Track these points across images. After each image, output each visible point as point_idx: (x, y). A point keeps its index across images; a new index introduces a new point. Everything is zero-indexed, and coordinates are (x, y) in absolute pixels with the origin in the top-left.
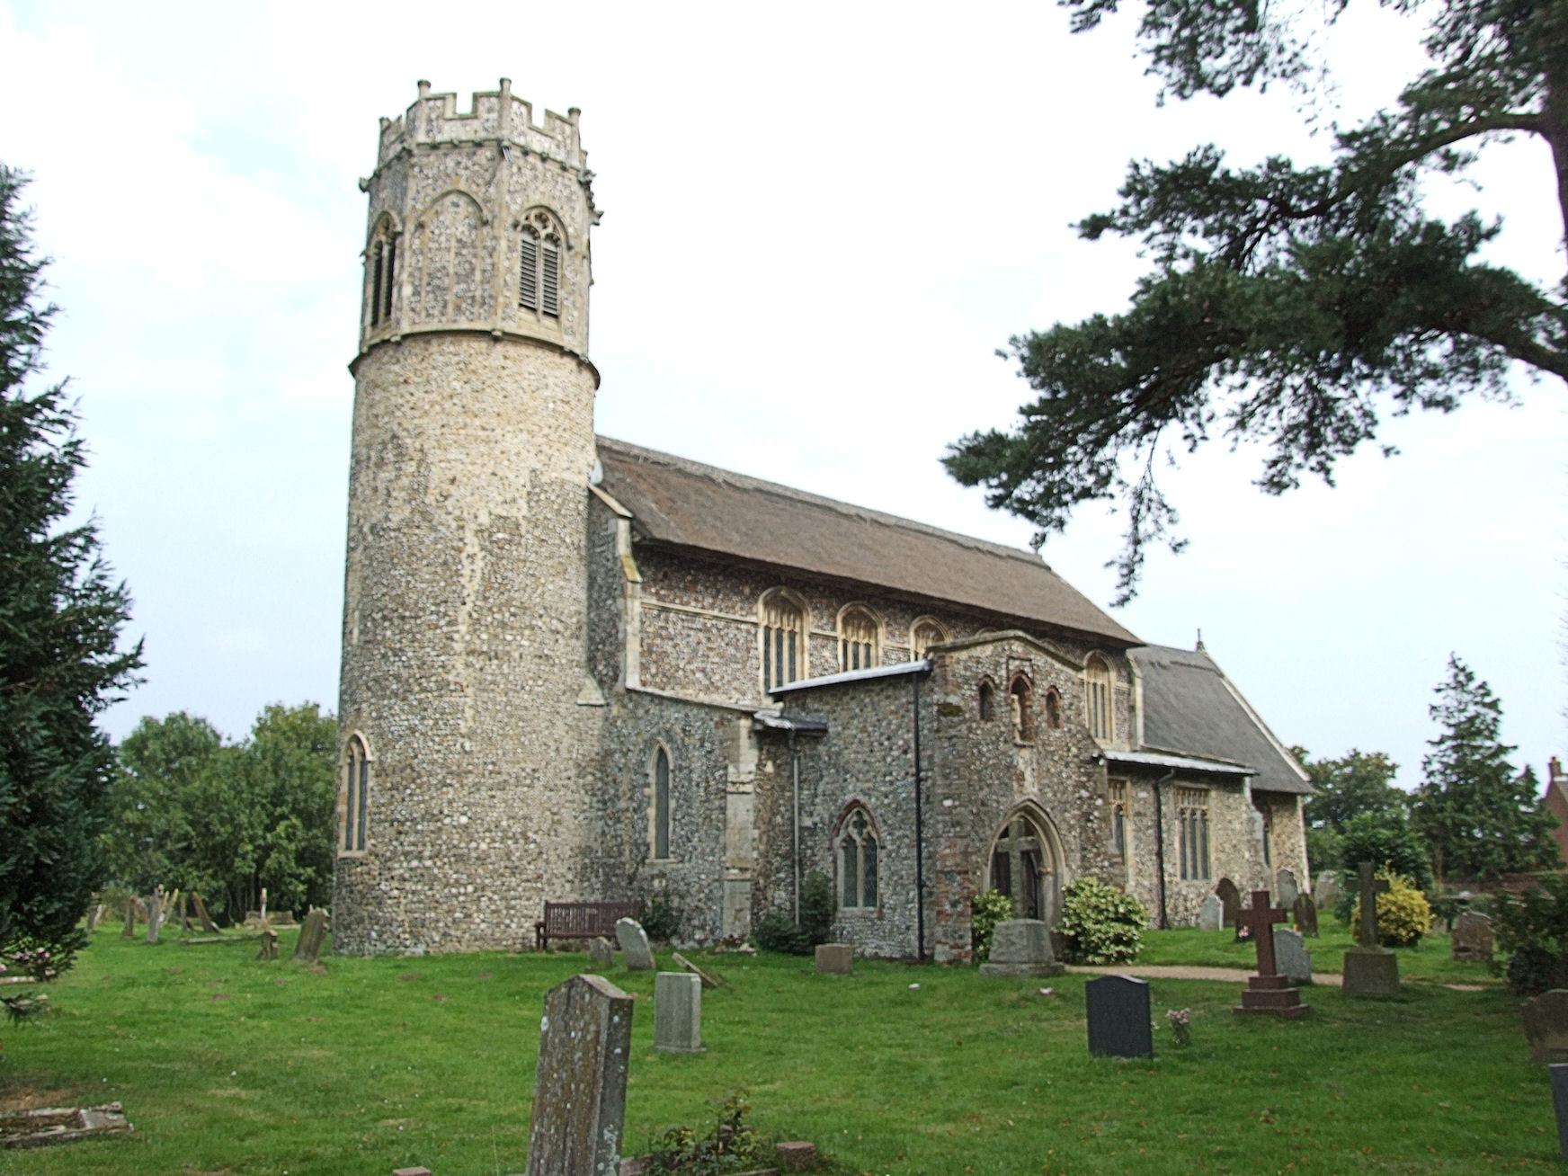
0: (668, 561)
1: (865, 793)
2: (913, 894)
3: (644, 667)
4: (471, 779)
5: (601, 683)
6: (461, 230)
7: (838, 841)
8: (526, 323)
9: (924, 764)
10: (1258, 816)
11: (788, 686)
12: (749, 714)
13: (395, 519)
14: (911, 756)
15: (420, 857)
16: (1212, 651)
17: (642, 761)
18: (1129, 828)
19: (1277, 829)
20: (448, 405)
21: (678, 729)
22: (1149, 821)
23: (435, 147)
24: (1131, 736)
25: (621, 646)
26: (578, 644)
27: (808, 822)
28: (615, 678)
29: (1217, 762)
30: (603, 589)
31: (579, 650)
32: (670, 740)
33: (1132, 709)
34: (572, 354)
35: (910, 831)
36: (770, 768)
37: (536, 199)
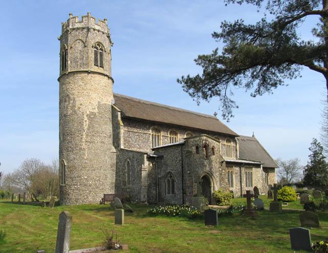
0: (130, 121)
1: (171, 170)
2: (182, 191)
3: (125, 144)
4: (87, 169)
5: (115, 148)
6: (80, 48)
7: (166, 180)
8: (96, 69)
9: (184, 164)
10: (264, 173)
11: (154, 147)
12: (146, 154)
13: (69, 113)
14: (181, 162)
15: (77, 185)
16: (257, 137)
17: (127, 162)
18: (234, 176)
19: (270, 176)
20: (79, 88)
21: (131, 157)
22: (239, 174)
23: (74, 29)
24: (236, 156)
25: (119, 139)
26: (110, 139)
27: (159, 176)
28: (118, 146)
29: (255, 161)
30: (116, 128)
31: (111, 140)
32: (130, 159)
33: (236, 150)
34: (107, 76)
35: (181, 178)
36: (151, 165)
37: (97, 40)
